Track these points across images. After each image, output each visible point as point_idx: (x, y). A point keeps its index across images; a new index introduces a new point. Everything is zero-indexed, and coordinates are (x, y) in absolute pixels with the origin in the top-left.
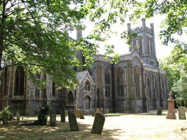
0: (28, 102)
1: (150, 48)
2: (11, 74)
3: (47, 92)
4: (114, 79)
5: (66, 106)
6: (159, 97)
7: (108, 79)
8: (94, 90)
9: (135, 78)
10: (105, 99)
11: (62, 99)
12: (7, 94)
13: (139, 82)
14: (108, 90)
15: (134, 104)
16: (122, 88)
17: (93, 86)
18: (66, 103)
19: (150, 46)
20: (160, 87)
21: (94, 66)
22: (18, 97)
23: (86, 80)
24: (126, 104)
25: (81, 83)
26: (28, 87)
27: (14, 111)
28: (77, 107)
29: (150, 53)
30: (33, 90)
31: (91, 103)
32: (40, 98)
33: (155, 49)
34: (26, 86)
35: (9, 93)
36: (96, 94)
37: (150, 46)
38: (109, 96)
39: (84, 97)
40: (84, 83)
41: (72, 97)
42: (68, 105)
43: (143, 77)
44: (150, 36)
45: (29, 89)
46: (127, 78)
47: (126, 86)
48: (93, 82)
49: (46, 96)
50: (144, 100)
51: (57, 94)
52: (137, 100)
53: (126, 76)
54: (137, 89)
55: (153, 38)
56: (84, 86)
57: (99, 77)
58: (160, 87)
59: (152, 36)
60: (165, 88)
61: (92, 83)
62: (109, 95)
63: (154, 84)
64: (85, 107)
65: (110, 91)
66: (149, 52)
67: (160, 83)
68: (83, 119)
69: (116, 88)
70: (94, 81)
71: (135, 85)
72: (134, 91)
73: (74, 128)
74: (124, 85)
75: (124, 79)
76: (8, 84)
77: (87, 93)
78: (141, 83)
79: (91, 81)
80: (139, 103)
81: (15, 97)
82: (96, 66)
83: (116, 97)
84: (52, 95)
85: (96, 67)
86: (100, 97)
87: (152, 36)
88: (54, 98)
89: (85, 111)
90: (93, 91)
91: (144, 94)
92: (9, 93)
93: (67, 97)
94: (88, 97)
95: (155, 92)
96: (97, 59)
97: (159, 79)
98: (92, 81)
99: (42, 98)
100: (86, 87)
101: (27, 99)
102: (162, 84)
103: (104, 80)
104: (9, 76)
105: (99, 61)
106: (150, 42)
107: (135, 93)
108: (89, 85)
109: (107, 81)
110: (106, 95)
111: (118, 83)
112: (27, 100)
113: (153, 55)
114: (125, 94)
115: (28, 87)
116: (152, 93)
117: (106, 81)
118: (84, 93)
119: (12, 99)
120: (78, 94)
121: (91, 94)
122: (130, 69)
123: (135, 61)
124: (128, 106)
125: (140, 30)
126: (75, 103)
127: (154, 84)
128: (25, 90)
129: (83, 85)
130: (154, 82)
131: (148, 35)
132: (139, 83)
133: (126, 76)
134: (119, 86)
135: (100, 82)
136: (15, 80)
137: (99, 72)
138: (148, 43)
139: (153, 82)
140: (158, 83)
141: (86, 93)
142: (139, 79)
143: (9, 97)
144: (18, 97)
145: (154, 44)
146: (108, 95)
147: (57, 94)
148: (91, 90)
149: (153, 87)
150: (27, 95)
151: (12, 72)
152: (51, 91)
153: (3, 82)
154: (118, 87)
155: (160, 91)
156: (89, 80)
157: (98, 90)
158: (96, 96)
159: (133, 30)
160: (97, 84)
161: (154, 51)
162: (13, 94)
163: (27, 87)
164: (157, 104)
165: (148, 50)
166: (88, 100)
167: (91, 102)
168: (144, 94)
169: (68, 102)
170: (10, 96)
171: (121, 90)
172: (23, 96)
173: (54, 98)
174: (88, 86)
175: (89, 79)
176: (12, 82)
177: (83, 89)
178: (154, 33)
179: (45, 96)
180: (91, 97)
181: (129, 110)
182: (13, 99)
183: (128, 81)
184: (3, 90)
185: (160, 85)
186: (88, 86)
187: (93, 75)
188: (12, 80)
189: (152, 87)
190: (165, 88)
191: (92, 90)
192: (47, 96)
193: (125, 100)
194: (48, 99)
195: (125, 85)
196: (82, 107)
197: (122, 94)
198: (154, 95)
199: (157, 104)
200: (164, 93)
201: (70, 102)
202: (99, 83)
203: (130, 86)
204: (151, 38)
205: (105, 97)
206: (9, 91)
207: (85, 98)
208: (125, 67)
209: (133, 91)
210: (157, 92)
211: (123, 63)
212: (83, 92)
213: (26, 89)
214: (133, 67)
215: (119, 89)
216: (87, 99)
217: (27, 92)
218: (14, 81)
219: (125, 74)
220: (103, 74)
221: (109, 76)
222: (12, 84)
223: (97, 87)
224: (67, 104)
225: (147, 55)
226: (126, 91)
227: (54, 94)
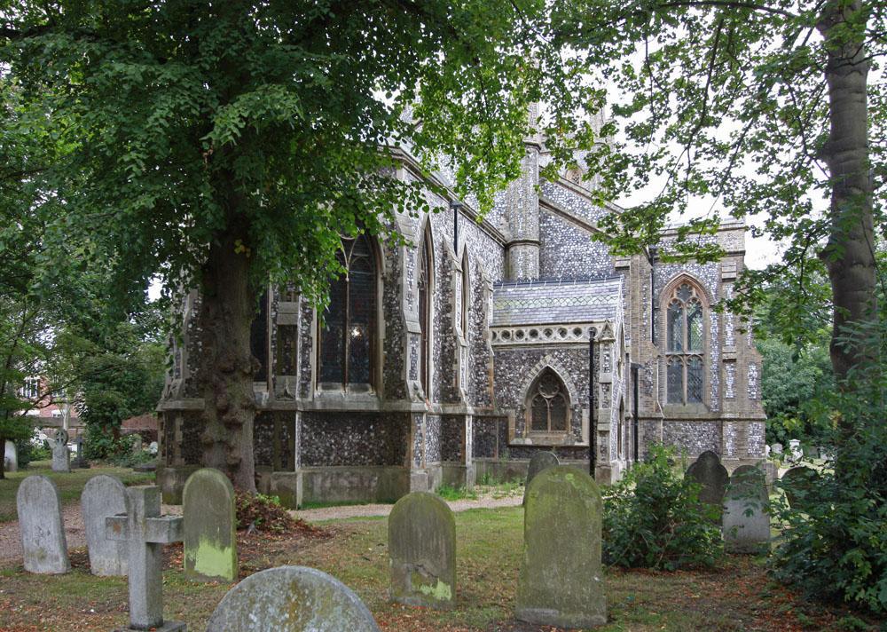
18: (512, 427)
42: (529, 442)
119: (312, 403)
182: (319, 406)
192: (410, 383)
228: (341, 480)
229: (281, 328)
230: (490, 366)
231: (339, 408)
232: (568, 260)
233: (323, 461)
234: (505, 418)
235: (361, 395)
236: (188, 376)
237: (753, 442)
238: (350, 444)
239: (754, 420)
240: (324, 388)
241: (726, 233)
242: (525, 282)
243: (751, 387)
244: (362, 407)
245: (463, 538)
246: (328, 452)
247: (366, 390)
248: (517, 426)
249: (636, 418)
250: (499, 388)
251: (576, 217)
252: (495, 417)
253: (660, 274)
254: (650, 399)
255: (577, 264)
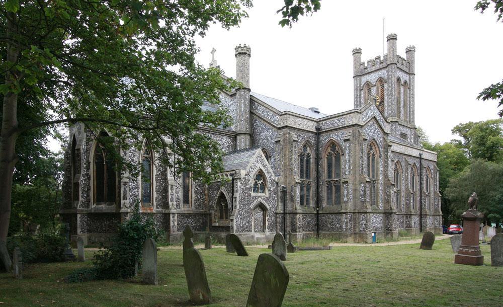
0: (125, 216)
1: (402, 105)
2: (83, 157)
3: (170, 197)
4: (320, 169)
5: (214, 224)
6: (418, 209)
7: (307, 166)
8: (276, 192)
9: (368, 165)
10: (299, 211)
11: (205, 211)
12: (78, 199)
13: (377, 174)
14: (305, 192)
15: (364, 222)
16: (338, 189)
17: (271, 183)
18: (213, 219)
19: (402, 100)
20: (421, 190)
21: (276, 140)
22: (104, 207)
23: (256, 170)
24: (347, 223)
25: (246, 175)
26: (125, 184)
27: (96, 238)
28: (235, 228)
29: (402, 115)
30: (138, 191)
31: (269, 219)
32: (155, 207)
33: (414, 106)
34: (120, 182)
35: (82, 197)
36: (280, 200)
37: (402, 100)
38: (307, 204)
39: (252, 206)
40: (252, 175)
41: (226, 205)
42: (217, 225)
43: (388, 164)
44: (404, 77)
45: (127, 189)
46: (350, 166)
47: (347, 182)
48: (273, 175)
49: (168, 203)
50: (388, 214)
51: (193, 200)
52: (371, 215)
53: (349, 160)
54: (372, 191)
55: (410, 81)
56: (252, 183)
57: (287, 164)
58: (421, 190)
59: (408, 78)
60: (432, 189)
61: (270, 176)
62: (308, 203)
63: (409, 180)
64: (255, 228)
65: (311, 195)
66: (399, 112)
67: (421, 179)
68: (244, 256)
69: (324, 188)
70: (275, 173)
71: (368, 180)
72: (365, 194)
73: (199, 293)
74: (343, 180)
75: (343, 167)
76: (79, 178)
77: (258, 197)
78: (381, 178)
79: (268, 172)
80: (376, 220)
81: (97, 206)
82: (279, 139)
83: (324, 206)
84: (181, 203)
85: (279, 141)
86: (289, 209)
87: (410, 77)
88: (184, 209)
89: (253, 237)
90: (273, 194)
91: (387, 201)
92: (81, 199)
93: (215, 206)
94: (261, 207)
95: (410, 198)
96: (282, 124)
97: (421, 170)
98: (271, 171)
99: (160, 209)
100: (256, 184)
101: (123, 210)
102: (427, 182)
103: (296, 170)
104: (80, 160)
105: (286, 127)
106: (404, 91)
107: (368, 199)
108: (265, 180)
109: (304, 171)
110: (302, 203)
111: (330, 176)
112: (123, 213)
113: (408, 120)
114: (345, 200)
115: (125, 184)
116: (403, 199)
117: (302, 171)
118: (253, 197)
119: (91, 210)
120: (238, 200)
121: (267, 199)
122: (357, 145)
123: (371, 126)
124: (351, 227)
125: (382, 63)
126: (232, 220)
127: (409, 180)
128: (117, 190)
129: (249, 180)
130: (409, 177)
131: (400, 74)
132: (377, 176)
133: (349, 160)
134: (333, 182)
135: (287, 175)
136: (95, 169)
137: (287, 153)
138: (399, 93)
139: (407, 177)
140: (417, 179)
141: (256, 198)
142: (377, 168)
143: (83, 207)
144: (104, 207)
145: (413, 94)
146: (305, 204)
147: (193, 200)
148: (267, 191)
149: (407, 189)
150: (122, 202)
151: (87, 151)
152: (180, 195)
153: (71, 174)
154: (329, 183)
155: (421, 197)
156: (263, 169)
157: (284, 192)
158: (280, 203)
159: (366, 65)
160: (282, 179)
161: (410, 111)
162: (92, 201)
163: (122, 184)
164: (413, 224)
165: (399, 108)
166: (262, 213)
167: (267, 218)
168: (387, 201)
169: (217, 217)
170: (87, 204)
171: (336, 193)
172: (114, 205)
173: (186, 209)
174: (261, 182)
175: (265, 166)
176: (87, 175)
177: (250, 189)
178: (413, 70)
179: (165, 205)
180: (268, 207)
181: (353, 236)
182: (93, 211)
183: (351, 172)
184: (71, 192)
185: (421, 184)
186: (261, 182)
187: (273, 159)
188: (88, 168)
189: (403, 188)
190: (432, 189)
191: (269, 190)
192: (170, 203)
193: (344, 213)
194: (173, 211)
195: (346, 180)
196: (247, 227)
197: (338, 201)
198: (408, 206)
199: (413, 224)
200: (429, 201)
201: (221, 218)
202: (286, 177)
203: (357, 182)
204: (406, 82)
205: (298, 207)
206: (80, 193)
207: (255, 208)
208: (345, 141)
209: (362, 193)
210: (413, 198)
211: (342, 131)
212: (250, 195)
213: (119, 188)
214: (365, 140)
215: (332, 189)
216: (258, 210)
217: (122, 195)
218: (92, 172)
219: (347, 157)
220: (295, 157)
221: (308, 162)
222: (89, 178)
223: (282, 186)
224: (215, 222)
225: (394, 119)
226: (347, 193)
227: (186, 200)
228: (102, 238)
229: (75, 183)
230: (206, 192)
231: (100, 212)
232: (263, 140)
233: (95, 231)
234: (210, 214)
235: (110, 207)
236: (65, 202)
237: (362, 224)
238: (105, 225)
239: (362, 213)
240: (97, 204)
241: (348, 115)
242: (243, 151)
243: (361, 195)
244: (109, 211)
245: (294, 287)
246: (97, 228)
247: (112, 204)
248: (214, 218)
249: (285, 213)
250: (209, 202)
251: (265, 119)
252: (207, 214)
253: (322, 140)
254: (293, 204)
255: (266, 141)
